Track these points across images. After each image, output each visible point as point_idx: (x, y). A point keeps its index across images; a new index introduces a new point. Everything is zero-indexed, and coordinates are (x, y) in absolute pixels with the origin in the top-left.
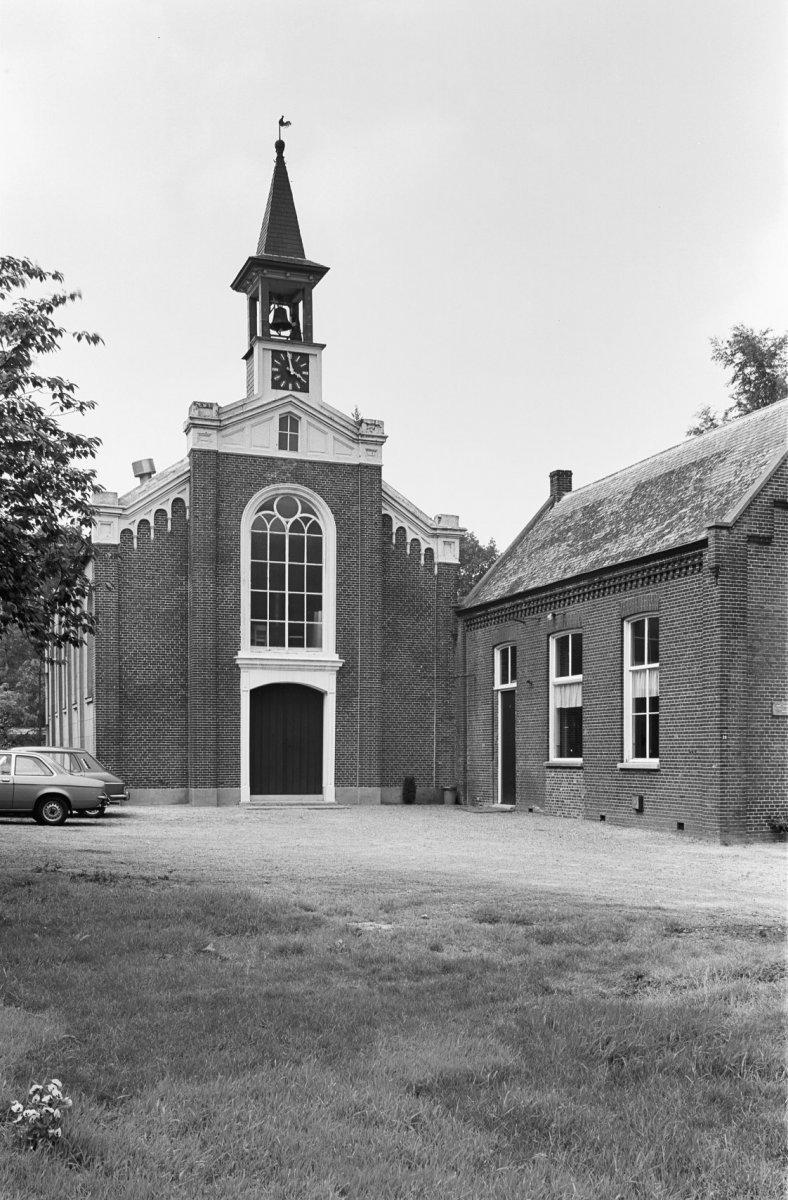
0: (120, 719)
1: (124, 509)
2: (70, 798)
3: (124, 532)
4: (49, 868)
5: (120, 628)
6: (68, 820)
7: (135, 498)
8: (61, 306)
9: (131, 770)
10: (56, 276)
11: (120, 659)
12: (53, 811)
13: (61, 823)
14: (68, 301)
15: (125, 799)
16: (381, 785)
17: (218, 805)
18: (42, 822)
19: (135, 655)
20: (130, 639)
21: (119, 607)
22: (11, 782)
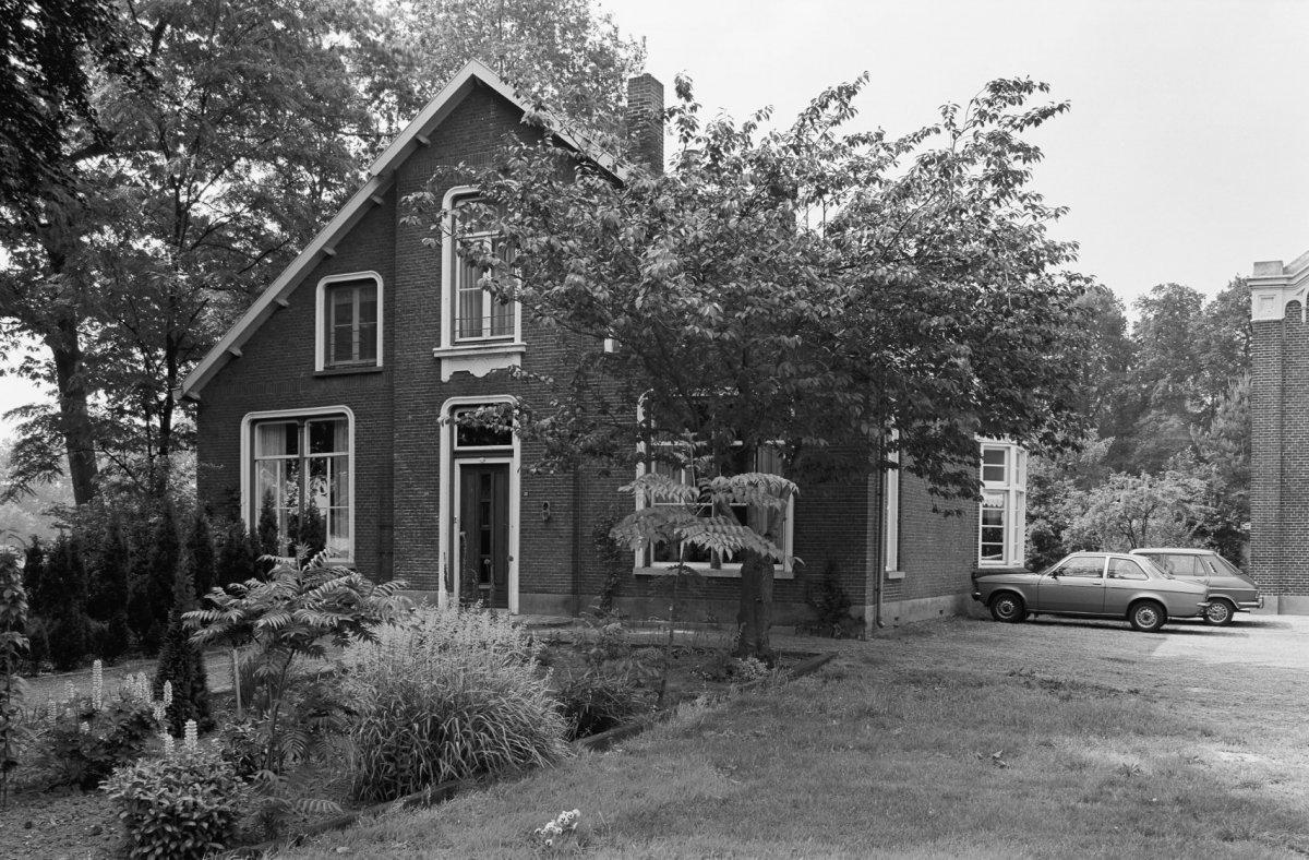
0: (1281, 517)
1: (1289, 279)
2: (1167, 606)
3: (1290, 304)
4: (1023, 672)
5: (1283, 414)
6: (1166, 627)
7: (1298, 269)
8: (1050, 117)
9: (1293, 575)
10: (1043, 87)
11: (1283, 448)
12: (1147, 617)
13: (1156, 630)
14: (1057, 113)
15: (1258, 607)
16: (864, 604)
17: (1279, 613)
18: (1136, 628)
19: (1301, 443)
20: (1296, 425)
21: (1283, 390)
22: (1103, 585)
